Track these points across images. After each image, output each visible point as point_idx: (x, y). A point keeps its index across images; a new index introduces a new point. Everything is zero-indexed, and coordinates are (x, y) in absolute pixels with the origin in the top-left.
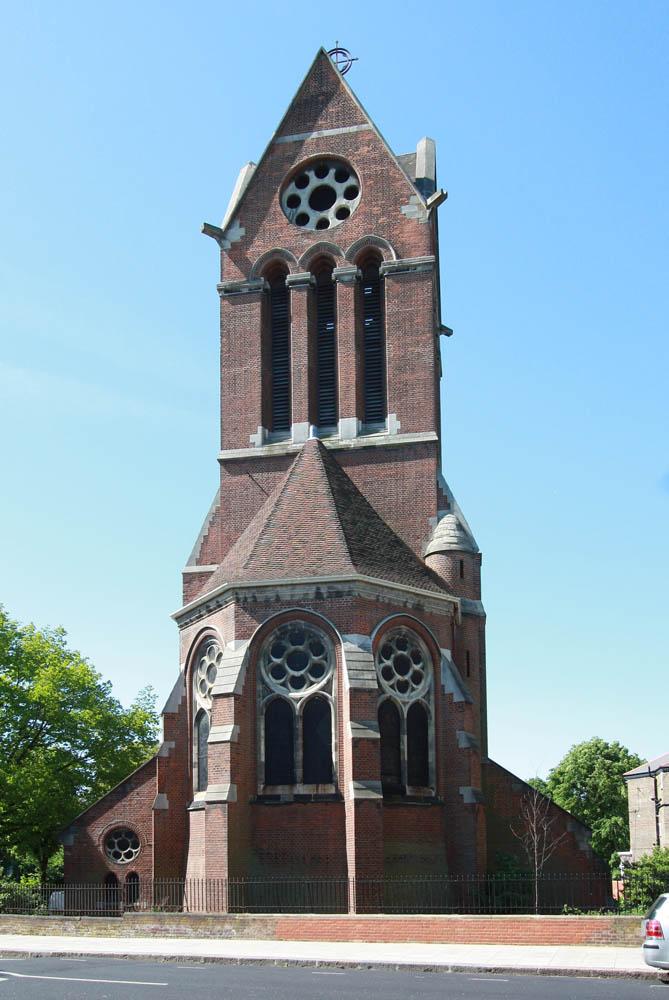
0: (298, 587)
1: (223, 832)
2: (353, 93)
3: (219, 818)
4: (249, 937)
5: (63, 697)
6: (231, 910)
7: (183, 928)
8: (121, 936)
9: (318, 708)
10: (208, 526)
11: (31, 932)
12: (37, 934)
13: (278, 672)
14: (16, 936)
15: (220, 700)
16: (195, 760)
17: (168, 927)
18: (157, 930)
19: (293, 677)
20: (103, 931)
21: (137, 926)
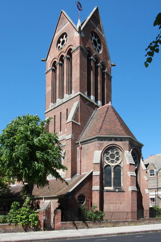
0: (137, 143)
1: (136, 198)
2: (103, 28)
3: (135, 195)
4: (130, 225)
5: (17, 148)
6: (150, 217)
7: (154, 221)
8: (141, 225)
9: (118, 169)
10: (76, 111)
11: (113, 226)
12: (116, 227)
13: (108, 159)
14: (108, 228)
15: (131, 165)
16: (104, 178)
17: (151, 221)
18: (149, 222)
19: (116, 159)
20: (136, 224)
21: (145, 222)
